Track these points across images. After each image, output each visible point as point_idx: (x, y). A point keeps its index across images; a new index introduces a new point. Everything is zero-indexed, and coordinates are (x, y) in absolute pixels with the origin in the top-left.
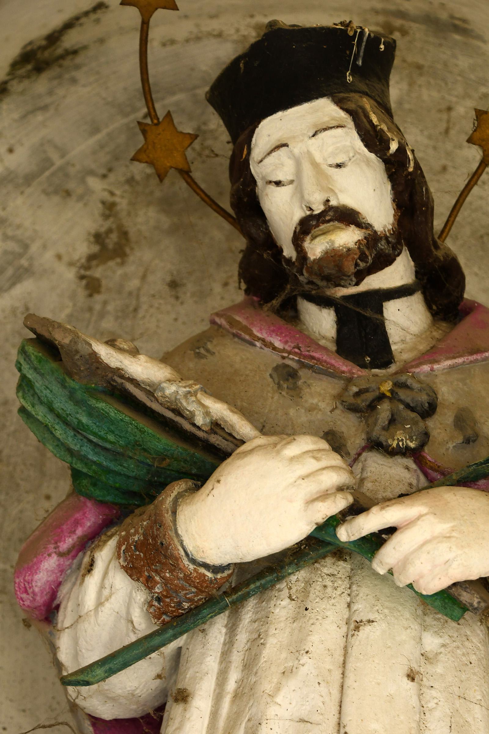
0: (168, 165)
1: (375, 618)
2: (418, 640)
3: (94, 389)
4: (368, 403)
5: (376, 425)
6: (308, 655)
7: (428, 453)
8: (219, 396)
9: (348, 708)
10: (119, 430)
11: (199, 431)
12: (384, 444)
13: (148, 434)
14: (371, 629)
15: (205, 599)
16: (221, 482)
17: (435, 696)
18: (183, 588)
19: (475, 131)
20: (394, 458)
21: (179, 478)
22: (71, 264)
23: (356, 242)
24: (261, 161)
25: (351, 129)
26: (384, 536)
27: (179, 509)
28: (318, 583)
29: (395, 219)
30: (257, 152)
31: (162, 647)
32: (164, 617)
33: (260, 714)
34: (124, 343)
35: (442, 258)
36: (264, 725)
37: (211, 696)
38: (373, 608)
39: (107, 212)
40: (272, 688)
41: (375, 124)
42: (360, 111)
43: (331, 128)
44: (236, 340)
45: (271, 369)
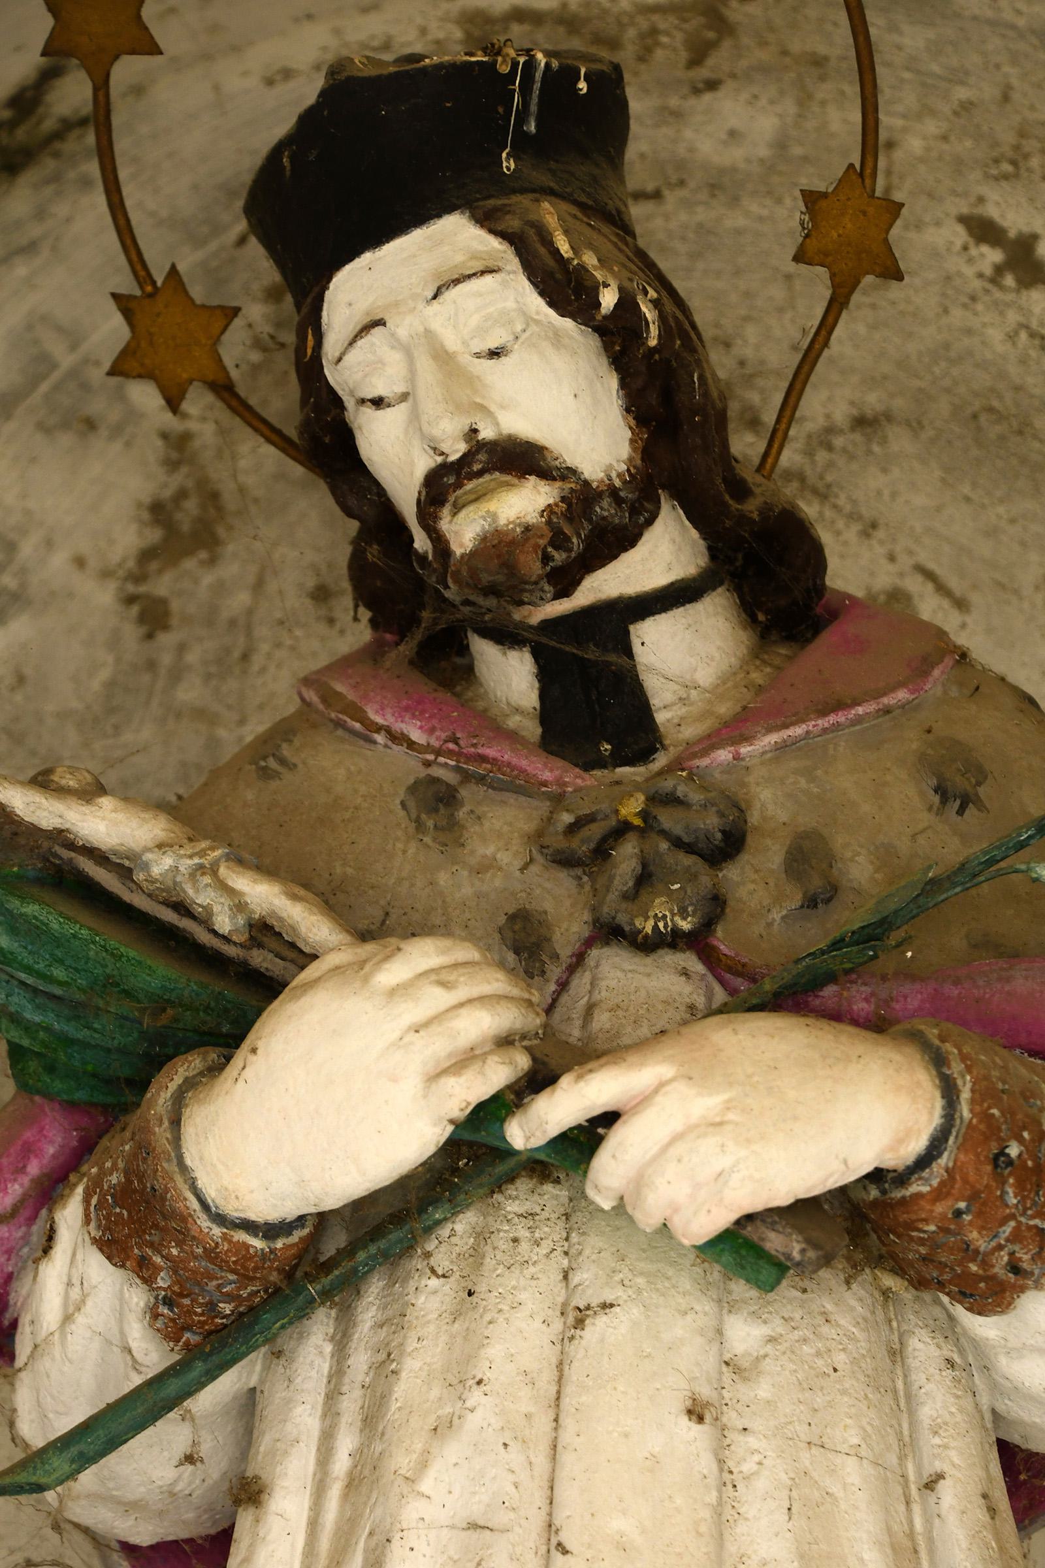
0: (185, 376)
1: (617, 1298)
2: (711, 1334)
3: (19, 877)
4: (592, 846)
5: (608, 891)
6: (483, 1388)
7: (722, 940)
8: (266, 869)
9: (567, 1494)
10: (73, 957)
11: (227, 946)
12: (627, 928)
13: (129, 960)
14: (608, 1321)
15: (266, 1291)
16: (259, 1052)
17: (756, 1447)
18: (211, 1277)
19: (807, 236)
20: (654, 956)
21: (190, 1048)
22: (106, 574)
23: (543, 511)
24: (340, 360)
25: (514, 272)
26: (600, 1131)
27: (186, 1113)
28: (502, 1234)
29: (634, 449)
30: (332, 344)
31: (185, 1399)
32: (187, 1335)
33: (389, 1520)
34: (68, 776)
35: (755, 516)
36: (396, 1542)
37: (309, 1488)
38: (611, 1278)
39: (174, 455)
40: (411, 1464)
41: (565, 256)
42: (531, 232)
43: (469, 277)
44: (340, 732)
45: (404, 789)
